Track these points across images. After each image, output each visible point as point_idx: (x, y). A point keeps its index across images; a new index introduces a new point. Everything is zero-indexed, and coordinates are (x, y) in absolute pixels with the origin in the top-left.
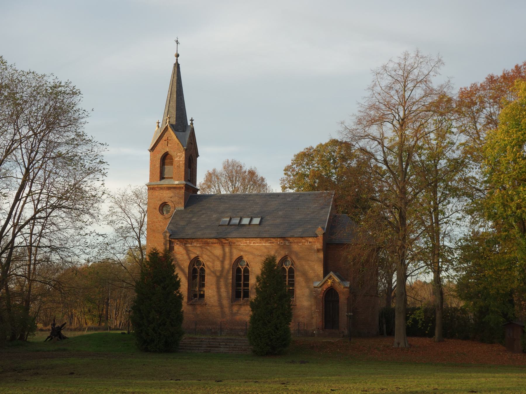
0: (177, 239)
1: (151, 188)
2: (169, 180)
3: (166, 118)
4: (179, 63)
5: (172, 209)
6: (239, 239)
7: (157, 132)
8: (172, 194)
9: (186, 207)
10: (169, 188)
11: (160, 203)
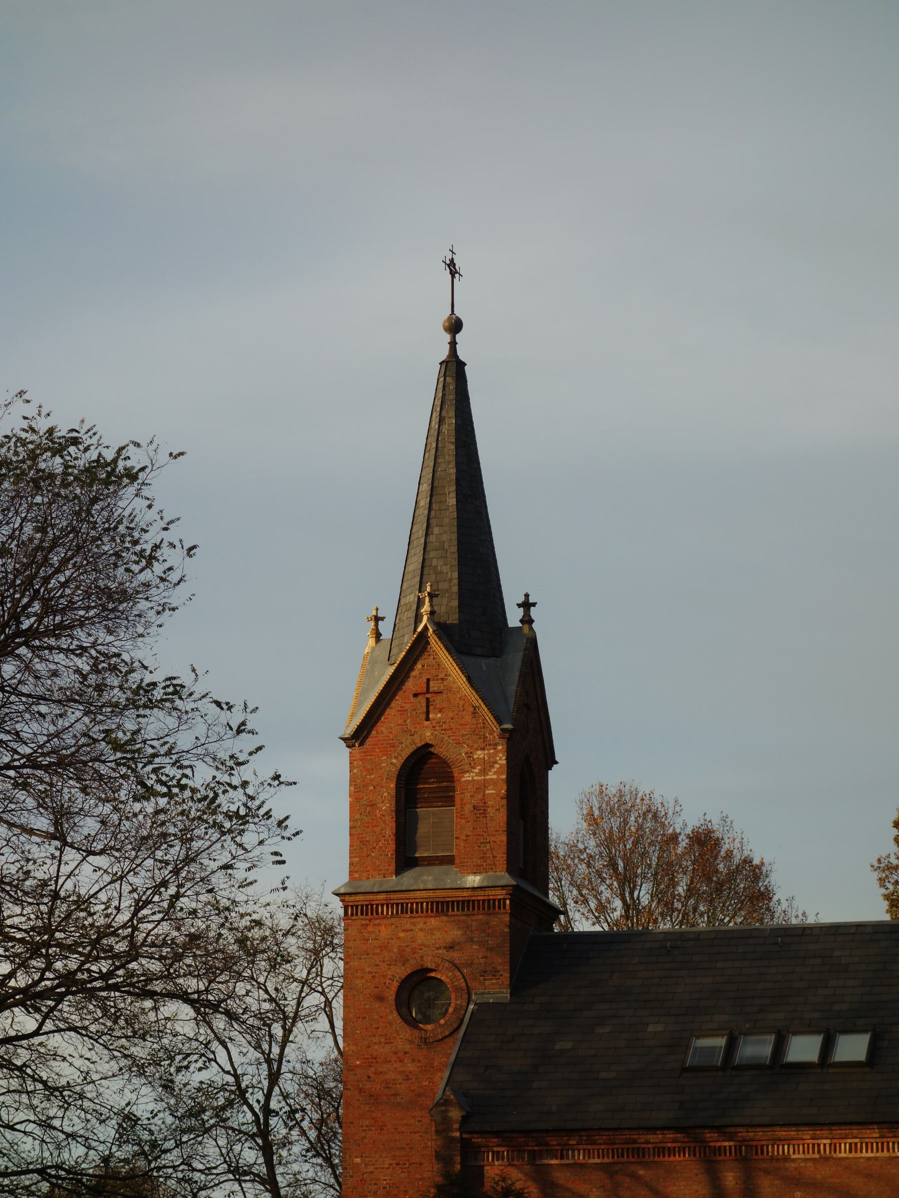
0: (498, 1134)
1: (357, 905)
2: (437, 869)
3: (412, 598)
4: (462, 356)
5: (455, 1001)
6: (782, 1133)
7: (371, 662)
8: (455, 934)
9: (516, 988)
10: (441, 907)
11: (401, 972)
